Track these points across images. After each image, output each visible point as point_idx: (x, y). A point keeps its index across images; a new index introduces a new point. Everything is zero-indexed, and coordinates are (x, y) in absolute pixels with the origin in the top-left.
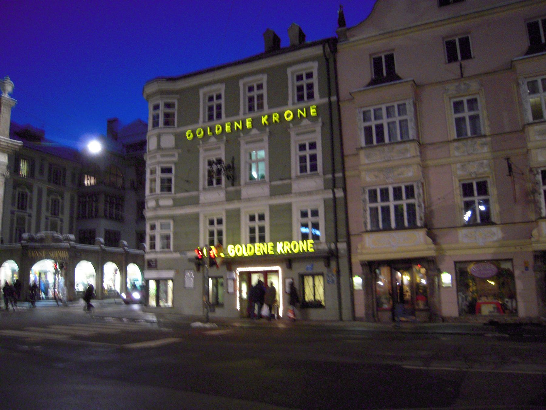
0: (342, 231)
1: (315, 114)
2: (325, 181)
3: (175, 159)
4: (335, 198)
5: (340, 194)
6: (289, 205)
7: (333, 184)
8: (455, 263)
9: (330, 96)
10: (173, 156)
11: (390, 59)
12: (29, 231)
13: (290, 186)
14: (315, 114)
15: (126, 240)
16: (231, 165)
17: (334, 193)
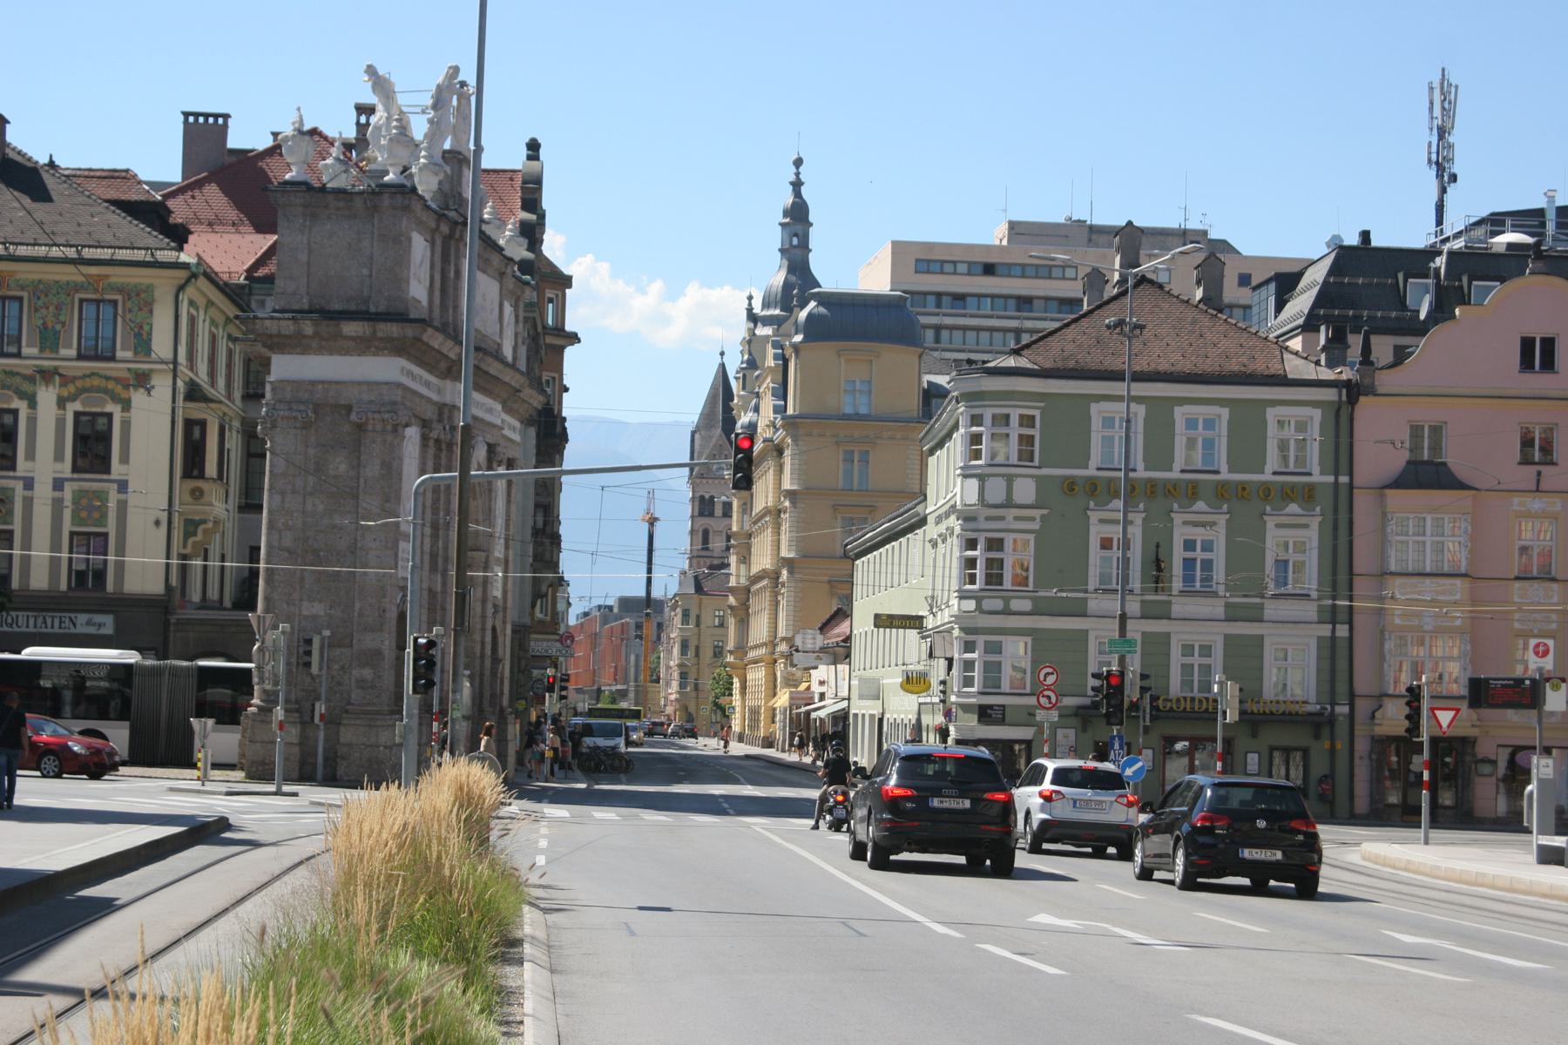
0: (1342, 688)
1: (1250, 756)
2: (1321, 609)
3: (1036, 526)
4: (1333, 638)
5: (1342, 631)
6: (1168, 635)
7: (1332, 616)
8: (186, 115)
9: (1336, 474)
10: (1033, 519)
11: (1436, 430)
12: (323, 639)
13: (1261, 607)
14: (1250, 756)
15: (76, 754)
16: (468, 75)
17: (1334, 630)
